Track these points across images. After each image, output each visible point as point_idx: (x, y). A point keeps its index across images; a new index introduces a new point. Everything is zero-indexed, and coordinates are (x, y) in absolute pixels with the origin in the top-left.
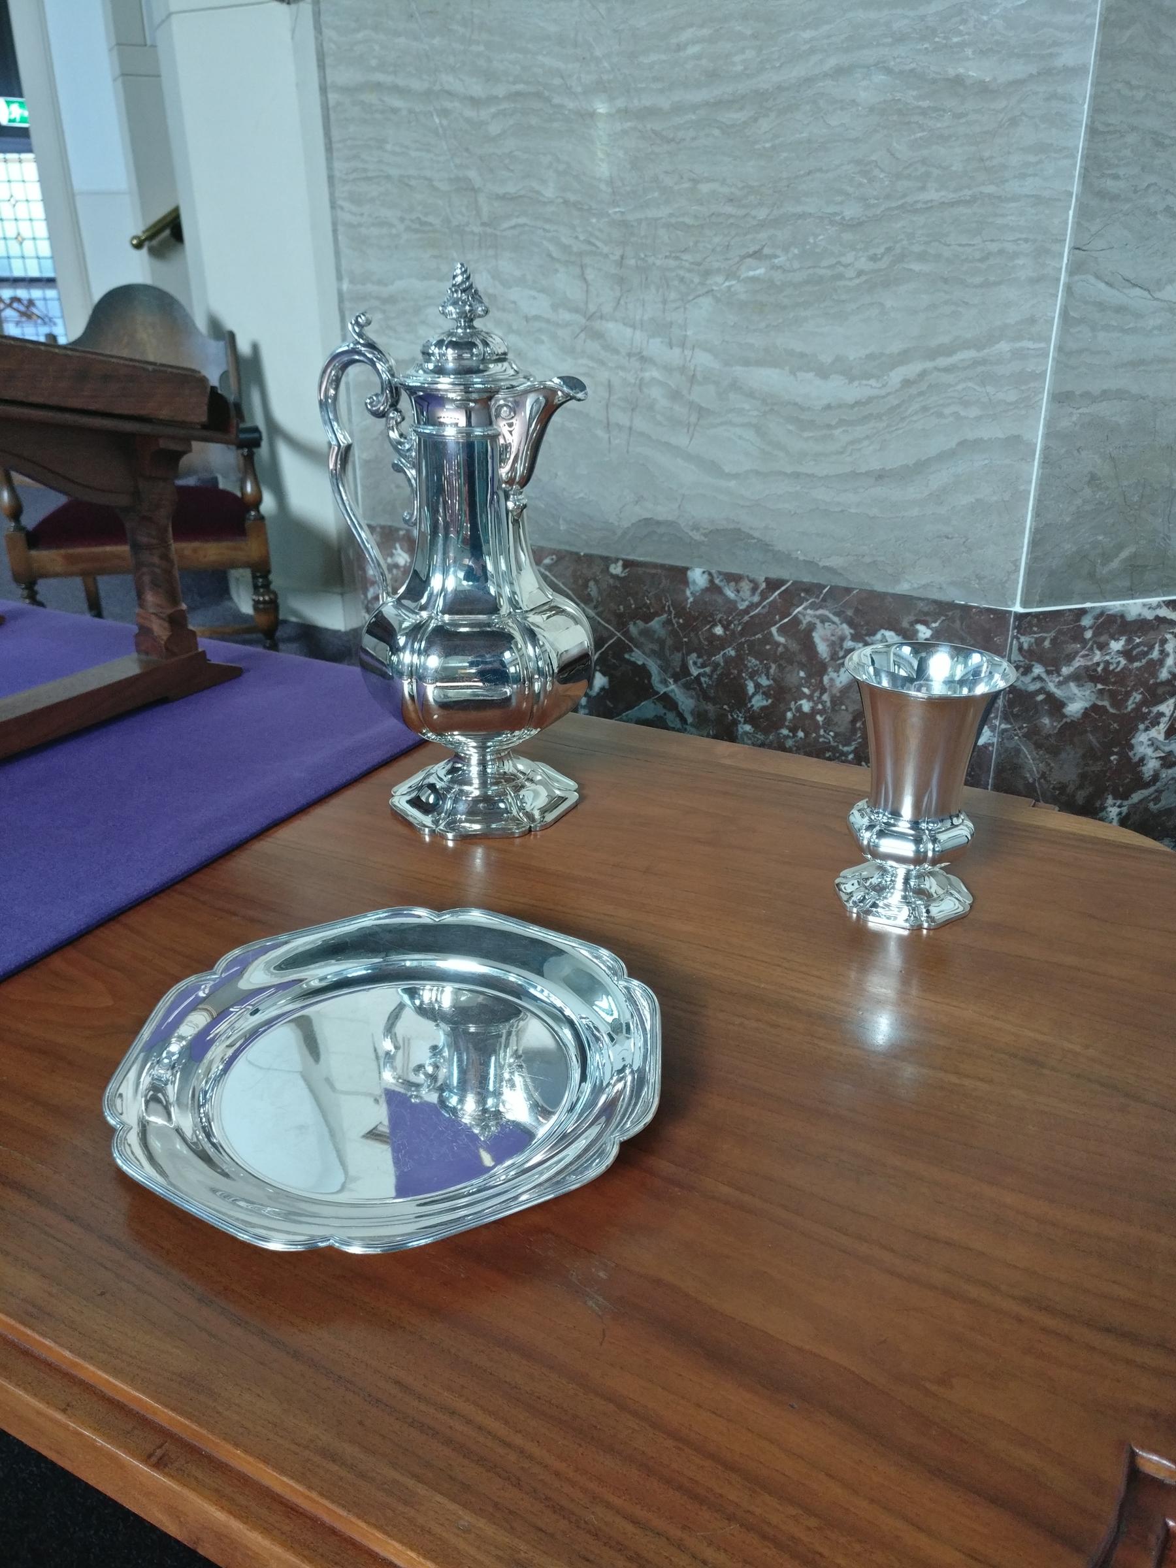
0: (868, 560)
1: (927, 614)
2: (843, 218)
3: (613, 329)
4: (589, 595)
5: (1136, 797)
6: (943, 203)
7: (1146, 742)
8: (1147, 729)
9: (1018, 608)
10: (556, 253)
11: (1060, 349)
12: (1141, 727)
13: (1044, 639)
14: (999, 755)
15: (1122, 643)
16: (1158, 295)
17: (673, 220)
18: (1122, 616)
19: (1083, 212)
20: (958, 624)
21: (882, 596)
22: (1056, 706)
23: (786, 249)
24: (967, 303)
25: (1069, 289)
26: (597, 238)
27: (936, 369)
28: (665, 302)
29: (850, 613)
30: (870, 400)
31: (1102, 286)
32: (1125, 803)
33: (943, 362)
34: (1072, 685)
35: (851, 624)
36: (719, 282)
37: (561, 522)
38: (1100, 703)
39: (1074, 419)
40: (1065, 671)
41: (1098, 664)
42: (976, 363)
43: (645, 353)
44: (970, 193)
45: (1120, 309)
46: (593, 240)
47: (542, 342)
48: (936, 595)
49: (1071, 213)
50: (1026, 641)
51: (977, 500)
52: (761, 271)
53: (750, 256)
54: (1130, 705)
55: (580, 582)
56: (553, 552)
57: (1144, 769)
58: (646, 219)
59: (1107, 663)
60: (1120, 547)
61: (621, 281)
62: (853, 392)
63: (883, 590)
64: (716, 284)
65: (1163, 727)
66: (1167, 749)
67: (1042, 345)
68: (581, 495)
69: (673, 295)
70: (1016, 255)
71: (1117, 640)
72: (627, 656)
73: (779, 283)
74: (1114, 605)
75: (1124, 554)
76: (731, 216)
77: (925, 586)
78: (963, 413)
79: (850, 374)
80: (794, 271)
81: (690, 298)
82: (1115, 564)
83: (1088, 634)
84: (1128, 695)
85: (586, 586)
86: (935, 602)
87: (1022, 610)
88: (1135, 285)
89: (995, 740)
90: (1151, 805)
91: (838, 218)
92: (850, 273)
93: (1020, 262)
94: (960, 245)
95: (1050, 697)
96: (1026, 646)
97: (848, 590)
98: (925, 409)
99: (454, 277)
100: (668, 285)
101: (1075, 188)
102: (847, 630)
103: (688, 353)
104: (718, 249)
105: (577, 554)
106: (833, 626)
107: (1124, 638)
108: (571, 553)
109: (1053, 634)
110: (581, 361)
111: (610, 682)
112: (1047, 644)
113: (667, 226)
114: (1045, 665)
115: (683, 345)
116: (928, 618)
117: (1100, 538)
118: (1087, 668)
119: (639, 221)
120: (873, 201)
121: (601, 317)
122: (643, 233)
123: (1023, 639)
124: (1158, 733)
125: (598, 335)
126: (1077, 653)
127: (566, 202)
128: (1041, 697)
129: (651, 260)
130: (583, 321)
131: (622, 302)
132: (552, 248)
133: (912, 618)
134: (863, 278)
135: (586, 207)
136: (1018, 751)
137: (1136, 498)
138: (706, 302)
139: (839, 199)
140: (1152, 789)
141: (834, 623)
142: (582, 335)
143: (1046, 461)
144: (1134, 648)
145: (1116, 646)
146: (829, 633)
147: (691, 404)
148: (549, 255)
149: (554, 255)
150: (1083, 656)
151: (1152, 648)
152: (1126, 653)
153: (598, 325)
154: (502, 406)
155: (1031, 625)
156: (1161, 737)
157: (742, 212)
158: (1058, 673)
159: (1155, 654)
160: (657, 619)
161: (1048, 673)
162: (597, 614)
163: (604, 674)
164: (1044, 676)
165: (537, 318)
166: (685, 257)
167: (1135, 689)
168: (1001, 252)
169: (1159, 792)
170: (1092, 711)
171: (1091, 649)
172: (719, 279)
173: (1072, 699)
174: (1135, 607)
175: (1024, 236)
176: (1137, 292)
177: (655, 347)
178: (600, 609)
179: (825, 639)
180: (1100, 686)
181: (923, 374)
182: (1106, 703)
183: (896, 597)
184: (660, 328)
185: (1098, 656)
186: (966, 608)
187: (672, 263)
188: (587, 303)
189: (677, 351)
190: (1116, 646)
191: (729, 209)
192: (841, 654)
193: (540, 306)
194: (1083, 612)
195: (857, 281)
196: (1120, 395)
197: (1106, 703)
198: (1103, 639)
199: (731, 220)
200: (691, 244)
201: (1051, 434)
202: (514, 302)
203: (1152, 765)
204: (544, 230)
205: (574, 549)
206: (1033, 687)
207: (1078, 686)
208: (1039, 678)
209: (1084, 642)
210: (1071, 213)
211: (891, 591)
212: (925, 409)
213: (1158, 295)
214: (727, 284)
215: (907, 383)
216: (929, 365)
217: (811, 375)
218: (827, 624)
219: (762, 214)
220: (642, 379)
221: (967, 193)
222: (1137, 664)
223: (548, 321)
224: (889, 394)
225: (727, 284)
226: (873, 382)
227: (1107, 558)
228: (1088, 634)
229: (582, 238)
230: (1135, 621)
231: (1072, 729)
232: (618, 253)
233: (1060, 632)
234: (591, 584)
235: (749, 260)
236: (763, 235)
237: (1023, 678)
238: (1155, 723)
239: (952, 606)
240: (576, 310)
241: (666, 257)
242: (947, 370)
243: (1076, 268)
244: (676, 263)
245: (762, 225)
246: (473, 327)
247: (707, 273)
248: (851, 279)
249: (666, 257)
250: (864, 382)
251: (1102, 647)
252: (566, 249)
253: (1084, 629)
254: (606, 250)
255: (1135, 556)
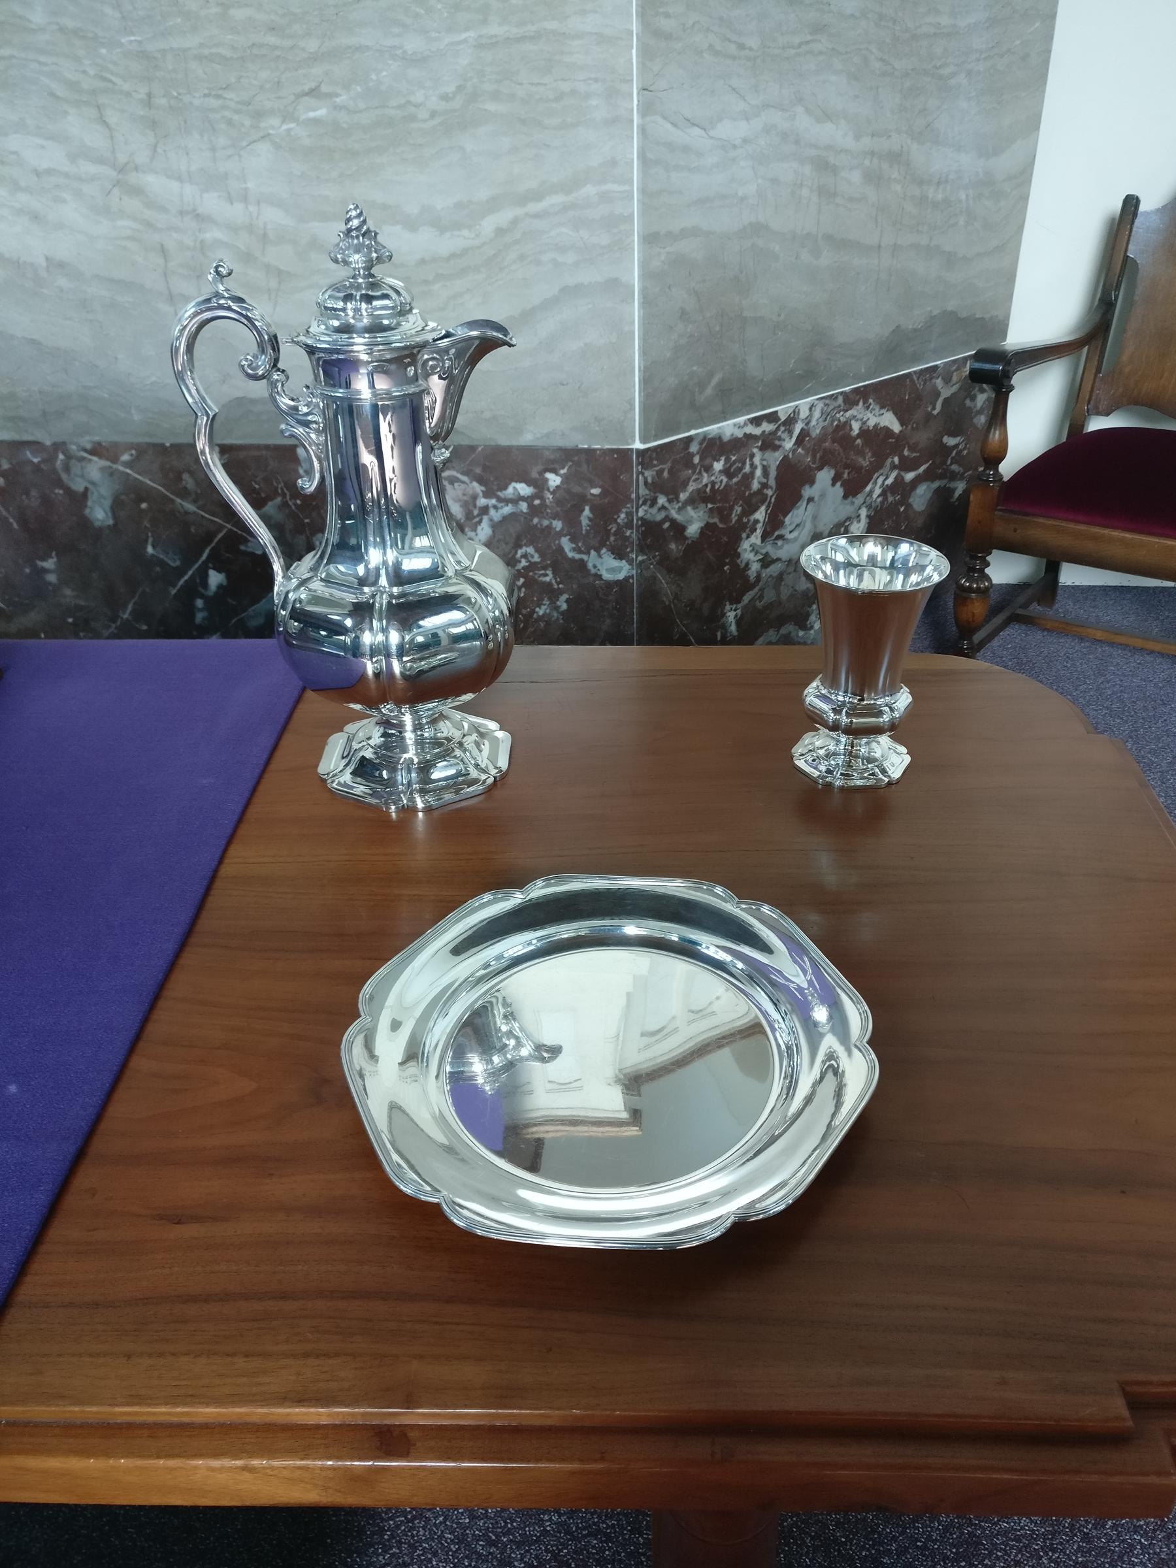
0: (487, 415)
1: (553, 462)
2: (405, 52)
3: (153, 182)
4: (185, 488)
5: (746, 599)
6: (508, 38)
7: (749, 549)
8: (748, 537)
9: (638, 445)
10: (60, 91)
11: (643, 191)
12: (744, 535)
13: (662, 471)
14: (639, 586)
15: (722, 462)
16: (712, 133)
17: (206, 52)
18: (720, 438)
19: (646, 53)
20: (584, 468)
21: (507, 450)
22: (679, 529)
23: (347, 87)
24: (548, 146)
25: (643, 130)
26: (112, 73)
27: (527, 214)
28: (213, 149)
29: (478, 471)
30: (465, 251)
31: (669, 126)
32: (739, 606)
33: (533, 207)
34: (689, 508)
35: (481, 481)
36: (273, 123)
37: (133, 411)
38: (712, 521)
39: (663, 257)
40: (683, 496)
41: (706, 485)
42: (565, 208)
43: (200, 211)
44: (533, 28)
45: (686, 149)
46: (108, 76)
47: (65, 201)
48: (560, 442)
49: (634, 51)
50: (649, 474)
51: (586, 344)
52: (321, 112)
53: (306, 94)
54: (734, 518)
55: (171, 475)
56: (131, 446)
57: (749, 572)
58: (172, 49)
59: (713, 483)
60: (711, 375)
61: (154, 124)
62: (447, 244)
63: (508, 443)
64: (273, 127)
65: (759, 532)
66: (764, 551)
67: (626, 187)
68: (154, 379)
69: (222, 141)
70: (588, 96)
71: (718, 460)
72: (242, 548)
73: (345, 126)
74: (712, 429)
75: (714, 381)
76: (276, 48)
77: (547, 435)
78: (560, 259)
79: (441, 226)
80: (361, 111)
81: (244, 144)
82: (709, 391)
83: (696, 460)
84: (731, 508)
85: (179, 479)
86: (560, 449)
87: (642, 446)
88: (694, 125)
89: (634, 572)
90: (759, 604)
91: (399, 52)
92: (423, 114)
93: (594, 102)
94: (532, 84)
95: (673, 522)
96: (650, 480)
97: (472, 448)
98: (522, 257)
99: (349, 220)
100: (214, 129)
101: (635, 26)
102: (477, 488)
103: (253, 208)
104: (268, 86)
105: (162, 445)
106: (463, 486)
107: (723, 458)
108: (155, 445)
109: (669, 464)
110: (120, 223)
111: (228, 578)
112: (666, 474)
113: (200, 58)
114: (666, 494)
115: (245, 199)
116: (556, 466)
117: (695, 368)
118: (698, 491)
119: (164, 52)
120: (433, 34)
121: (136, 169)
122: (170, 67)
123: (647, 473)
124: (756, 539)
125: (136, 191)
126: (689, 479)
127: (62, 29)
128: (666, 525)
129: (187, 99)
130: (114, 174)
131: (159, 150)
132: (54, 85)
133: (540, 467)
134: (438, 120)
135: (90, 35)
136: (655, 578)
137: (718, 328)
138: (264, 148)
139: (396, 30)
140: (756, 589)
141: (463, 482)
142: (116, 191)
143: (646, 302)
144: (731, 466)
145: (718, 466)
146: (460, 493)
147: (268, 268)
148: (52, 94)
149: (59, 94)
150: (695, 480)
151: (744, 463)
152: (726, 471)
153: (133, 178)
154: (427, 360)
155: (651, 459)
156: (759, 542)
157: (288, 43)
158: (677, 498)
159: (747, 469)
160: (270, 503)
161: (670, 501)
162: (198, 508)
163: (219, 571)
164: (667, 505)
165: (49, 172)
166: (229, 95)
167: (735, 502)
168: (574, 92)
169: (762, 590)
170: (707, 528)
171: (700, 473)
172: (275, 122)
173: (690, 522)
174: (729, 428)
175: (593, 76)
176: (696, 131)
177: (212, 203)
178: (201, 503)
179: (457, 500)
180: (710, 506)
181: (515, 222)
182: (716, 520)
183: (519, 448)
184: (213, 180)
185: (705, 479)
186: (590, 452)
187: (214, 103)
188: (113, 151)
189: (239, 207)
190: (718, 466)
191: (272, 40)
192: (476, 512)
193: (53, 157)
194: (689, 440)
195: (432, 123)
196: (694, 232)
197: (716, 520)
198: (708, 461)
199: (277, 53)
200: (233, 80)
201: (646, 275)
202: (15, 153)
203: (755, 567)
204: (40, 63)
205: (160, 441)
206: (660, 517)
207: (694, 509)
208: (663, 508)
209: (694, 467)
210: (634, 51)
211: (515, 443)
212: (522, 257)
213: (712, 133)
214: (285, 127)
215: (500, 232)
216: (519, 211)
217: (398, 228)
218: (456, 485)
219: (312, 45)
220: (202, 242)
221: (531, 29)
222: (735, 480)
223: (66, 175)
224: (484, 244)
225: (285, 127)
226: (465, 232)
227: (702, 386)
228: (696, 460)
229: (92, 72)
230: (730, 441)
231: (694, 549)
232: (142, 91)
233: (675, 462)
234: (186, 476)
235: (306, 98)
236: (317, 70)
237: (650, 510)
238: (754, 530)
239: (577, 451)
240: (101, 161)
241: (205, 96)
242: (537, 216)
243: (646, 109)
244: (220, 102)
245: (315, 58)
246: (372, 276)
247: (259, 115)
248: (425, 121)
249: (205, 96)
250: (457, 233)
251: (708, 469)
252: (73, 86)
253: (693, 455)
254: (126, 87)
255: (721, 383)
